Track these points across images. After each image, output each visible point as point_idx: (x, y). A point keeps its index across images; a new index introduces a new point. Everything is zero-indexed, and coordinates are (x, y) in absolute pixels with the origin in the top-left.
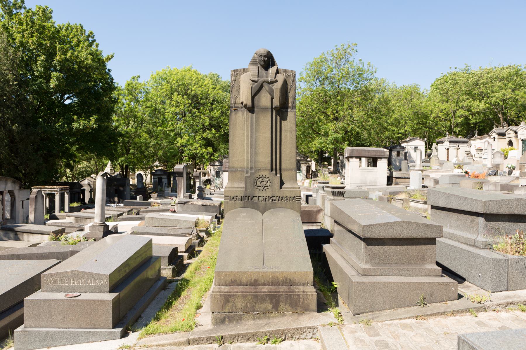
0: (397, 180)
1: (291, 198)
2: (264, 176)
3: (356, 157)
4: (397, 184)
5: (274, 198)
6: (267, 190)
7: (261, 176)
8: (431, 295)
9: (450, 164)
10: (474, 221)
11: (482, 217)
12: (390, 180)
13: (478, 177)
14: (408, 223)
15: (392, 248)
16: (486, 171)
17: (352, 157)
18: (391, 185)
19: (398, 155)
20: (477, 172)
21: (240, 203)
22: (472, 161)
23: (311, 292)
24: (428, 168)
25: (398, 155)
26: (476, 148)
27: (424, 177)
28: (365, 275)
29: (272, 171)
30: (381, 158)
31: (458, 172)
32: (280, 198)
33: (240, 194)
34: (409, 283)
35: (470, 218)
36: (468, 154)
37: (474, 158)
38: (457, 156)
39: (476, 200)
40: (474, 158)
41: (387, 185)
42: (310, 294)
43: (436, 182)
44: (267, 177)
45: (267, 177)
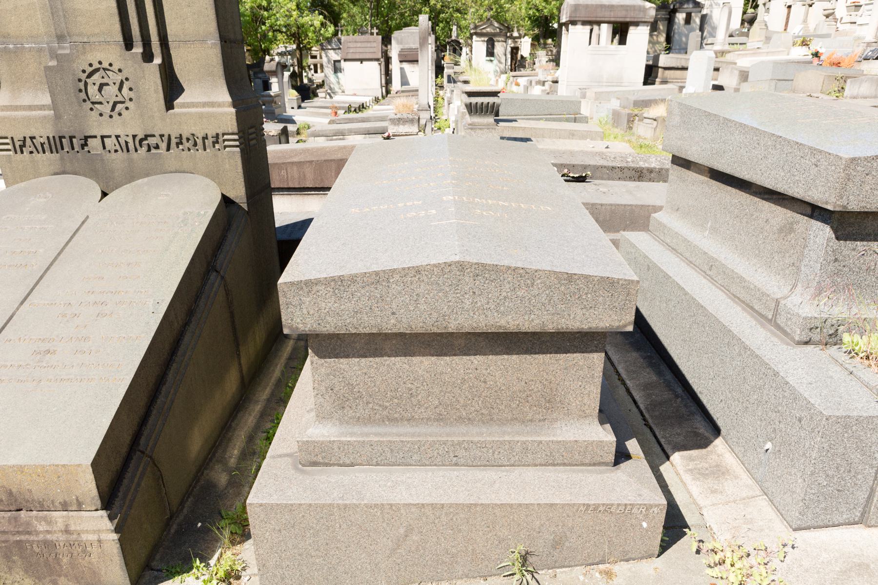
0: (667, 72)
1: (205, 138)
2: (105, 65)
3: (584, 23)
4: (664, 82)
5: (152, 141)
6: (124, 112)
7: (96, 65)
8: (557, 544)
9: (788, 37)
10: (791, 230)
11: (825, 221)
12: (651, 74)
13: (838, 64)
14: (482, 270)
15: (423, 364)
16: (859, 50)
17: (574, 23)
18: (653, 83)
19: (688, 20)
20: (839, 53)
21: (47, 159)
22: (833, 32)
23: (94, 532)
24: (742, 47)
25: (688, 20)
26: (848, 4)
27: (717, 66)
28: (315, 464)
29: (129, 45)
30: (636, 24)
31: (800, 53)
32: (174, 141)
33: (44, 132)
34: (470, 506)
35: (779, 214)
36: (827, 16)
37: (839, 25)
38: (805, 21)
39: (814, 151)
40: (839, 25)
41: (645, 83)
42: (92, 537)
43: (744, 76)
44: (115, 68)
45: (115, 68)
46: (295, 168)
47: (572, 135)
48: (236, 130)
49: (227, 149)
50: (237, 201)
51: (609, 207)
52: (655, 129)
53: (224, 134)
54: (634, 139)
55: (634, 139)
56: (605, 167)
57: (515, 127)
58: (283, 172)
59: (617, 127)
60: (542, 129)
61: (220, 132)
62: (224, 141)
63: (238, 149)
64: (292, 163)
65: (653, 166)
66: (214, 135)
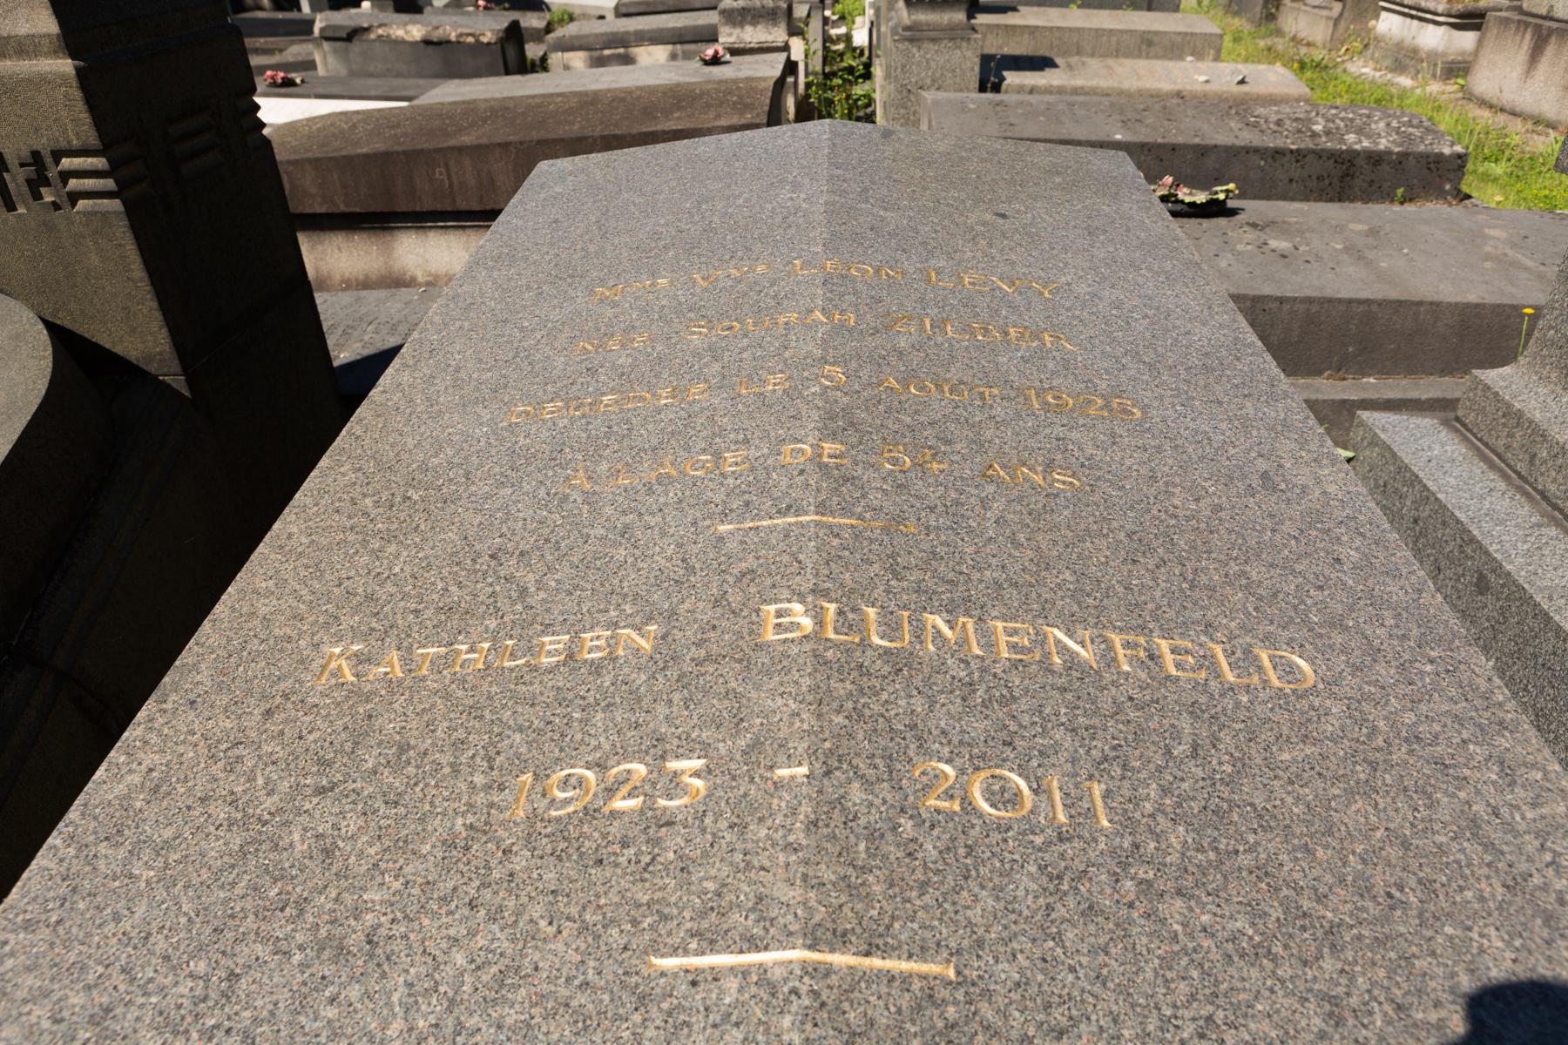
46: (467, 162)
47: (1148, 45)
48: (93, 140)
49: (82, 204)
50: (152, 368)
51: (1301, 307)
52: (1337, 21)
53: (57, 155)
54: (1280, 44)
55: (1280, 44)
56: (1256, 150)
57: (1014, 28)
58: (439, 173)
59: (1236, 14)
60: (1078, 29)
61: (43, 144)
62: (66, 176)
63: (115, 205)
64: (461, 150)
65: (1383, 144)
66: (25, 154)
